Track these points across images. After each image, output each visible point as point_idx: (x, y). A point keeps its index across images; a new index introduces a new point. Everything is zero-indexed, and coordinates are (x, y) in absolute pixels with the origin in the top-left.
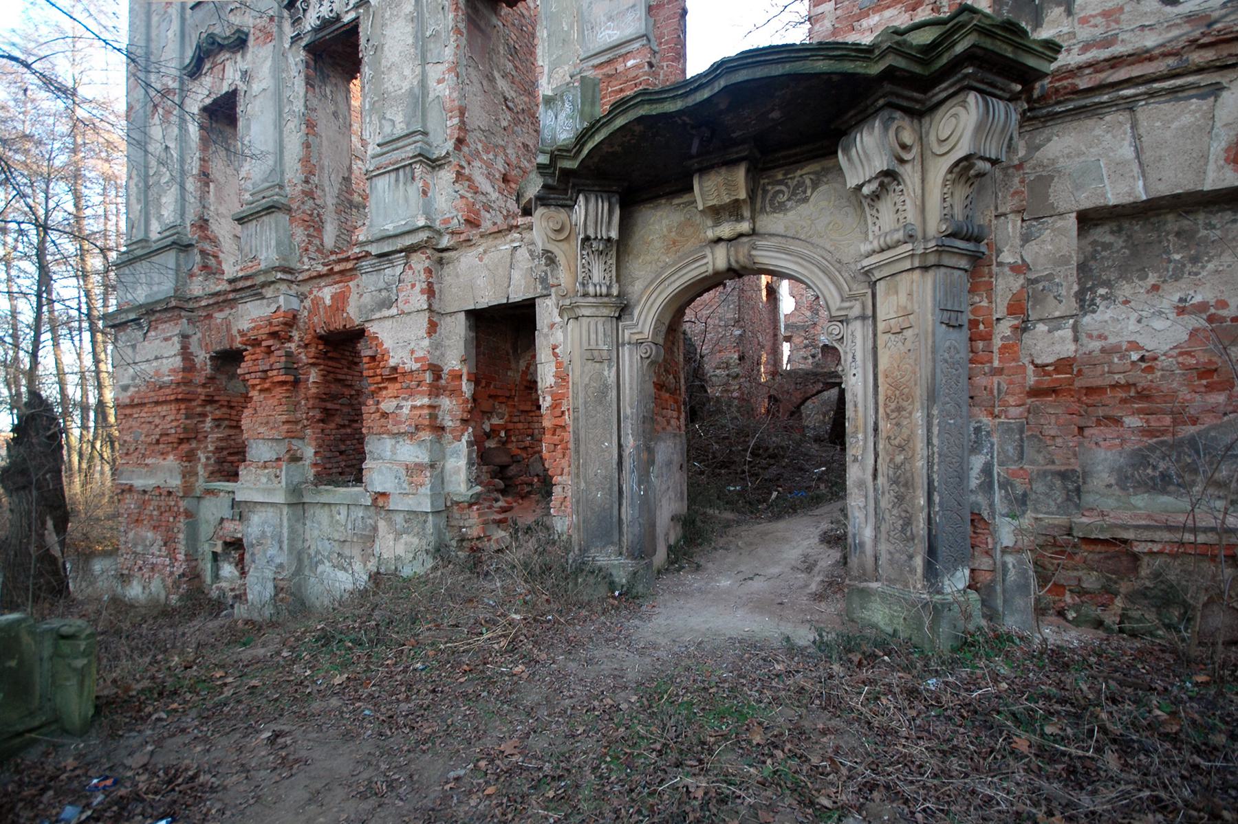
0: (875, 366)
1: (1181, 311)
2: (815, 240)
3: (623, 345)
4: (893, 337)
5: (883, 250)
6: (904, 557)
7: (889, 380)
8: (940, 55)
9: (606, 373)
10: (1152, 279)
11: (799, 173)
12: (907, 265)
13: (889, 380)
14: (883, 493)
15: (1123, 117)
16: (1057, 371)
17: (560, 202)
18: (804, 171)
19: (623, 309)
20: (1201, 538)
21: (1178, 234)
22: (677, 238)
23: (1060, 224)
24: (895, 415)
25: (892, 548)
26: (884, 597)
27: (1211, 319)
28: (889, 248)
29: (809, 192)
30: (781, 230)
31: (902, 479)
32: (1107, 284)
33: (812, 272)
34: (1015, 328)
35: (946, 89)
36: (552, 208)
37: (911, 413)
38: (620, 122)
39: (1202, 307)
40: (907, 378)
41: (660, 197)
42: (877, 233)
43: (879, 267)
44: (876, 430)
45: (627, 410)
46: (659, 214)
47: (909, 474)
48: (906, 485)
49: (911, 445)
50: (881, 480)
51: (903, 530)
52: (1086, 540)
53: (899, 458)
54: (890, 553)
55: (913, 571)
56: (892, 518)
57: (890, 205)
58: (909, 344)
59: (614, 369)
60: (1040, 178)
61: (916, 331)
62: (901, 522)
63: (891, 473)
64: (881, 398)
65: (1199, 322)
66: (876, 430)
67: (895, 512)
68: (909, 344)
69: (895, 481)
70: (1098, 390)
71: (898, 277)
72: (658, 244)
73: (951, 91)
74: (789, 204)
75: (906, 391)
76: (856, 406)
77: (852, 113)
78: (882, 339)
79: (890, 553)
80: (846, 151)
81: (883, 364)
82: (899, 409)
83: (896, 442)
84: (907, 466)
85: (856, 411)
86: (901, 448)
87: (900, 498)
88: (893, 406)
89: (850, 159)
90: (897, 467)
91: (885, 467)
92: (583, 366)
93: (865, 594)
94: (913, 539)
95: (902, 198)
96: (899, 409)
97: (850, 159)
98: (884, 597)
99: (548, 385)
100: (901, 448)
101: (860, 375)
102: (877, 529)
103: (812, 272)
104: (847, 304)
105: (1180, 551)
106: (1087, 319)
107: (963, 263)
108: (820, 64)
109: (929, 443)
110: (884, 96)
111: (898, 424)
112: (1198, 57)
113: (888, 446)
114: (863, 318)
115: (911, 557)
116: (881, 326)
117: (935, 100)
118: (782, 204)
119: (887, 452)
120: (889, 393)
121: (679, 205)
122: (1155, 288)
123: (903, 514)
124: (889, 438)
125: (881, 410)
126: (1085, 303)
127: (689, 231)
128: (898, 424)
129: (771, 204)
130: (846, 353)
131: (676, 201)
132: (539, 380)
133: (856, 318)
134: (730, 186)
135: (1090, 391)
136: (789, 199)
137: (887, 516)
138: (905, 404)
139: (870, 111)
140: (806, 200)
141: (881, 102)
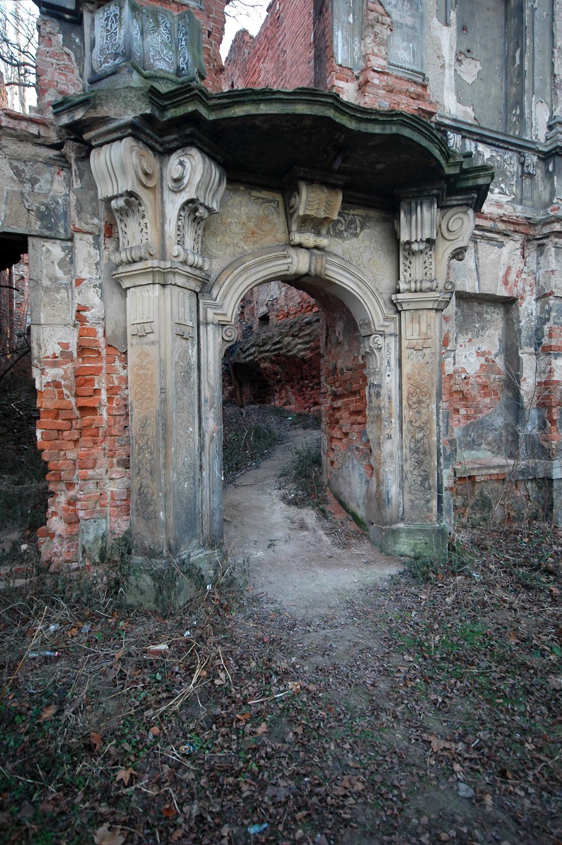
3: (207, 324)
4: (415, 352)
5: (416, 291)
6: (423, 502)
7: (411, 382)
8: (468, 179)
9: (190, 352)
10: (470, 336)
11: (352, 212)
12: (430, 305)
13: (411, 382)
14: (406, 460)
17: (150, 142)
18: (355, 212)
19: (204, 286)
20: (495, 471)
21: (478, 314)
22: (255, 229)
24: (415, 406)
25: (413, 497)
26: (409, 532)
27: (486, 360)
28: (421, 291)
29: (358, 229)
31: (421, 450)
33: (365, 293)
35: (458, 200)
36: (141, 145)
37: (428, 405)
38: (301, 109)
40: (426, 381)
41: (241, 182)
42: (408, 278)
43: (409, 302)
45: (206, 393)
47: (427, 446)
48: (425, 453)
49: (429, 426)
51: (422, 484)
53: (419, 436)
54: (411, 501)
55: (430, 510)
56: (413, 477)
57: (421, 262)
58: (427, 359)
59: (196, 348)
61: (433, 351)
62: (420, 479)
63: (412, 445)
64: (405, 394)
65: (482, 360)
67: (416, 472)
68: (427, 359)
71: (420, 312)
72: (235, 228)
73: (460, 202)
74: (345, 234)
75: (425, 390)
76: (390, 398)
77: (414, 189)
79: (411, 501)
80: (409, 213)
81: (406, 370)
82: (419, 402)
83: (417, 424)
84: (426, 441)
85: (390, 402)
86: (421, 428)
87: (420, 463)
88: (414, 399)
90: (418, 441)
91: (407, 442)
92: (174, 341)
93: (395, 533)
94: (430, 489)
95: (430, 260)
96: (419, 402)
98: (409, 532)
99: (50, 353)
100: (421, 428)
101: (393, 376)
102: (402, 488)
103: (365, 293)
104: (386, 323)
105: (491, 479)
107: (193, 285)
108: (437, 151)
109: (438, 425)
110: (439, 189)
111: (418, 412)
112: (501, 226)
113: (410, 427)
114: (396, 336)
115: (428, 501)
116: (405, 343)
117: (449, 203)
118: (341, 232)
119: (409, 431)
120: (411, 390)
121: (258, 198)
123: (422, 473)
124: (411, 422)
125: (404, 402)
127: (267, 227)
128: (418, 412)
130: (382, 358)
131: (255, 193)
132: (34, 345)
133: (391, 335)
134: (329, 206)
136: (345, 230)
137: (409, 476)
138: (424, 399)
139: (425, 194)
140: (356, 235)
141: (435, 192)
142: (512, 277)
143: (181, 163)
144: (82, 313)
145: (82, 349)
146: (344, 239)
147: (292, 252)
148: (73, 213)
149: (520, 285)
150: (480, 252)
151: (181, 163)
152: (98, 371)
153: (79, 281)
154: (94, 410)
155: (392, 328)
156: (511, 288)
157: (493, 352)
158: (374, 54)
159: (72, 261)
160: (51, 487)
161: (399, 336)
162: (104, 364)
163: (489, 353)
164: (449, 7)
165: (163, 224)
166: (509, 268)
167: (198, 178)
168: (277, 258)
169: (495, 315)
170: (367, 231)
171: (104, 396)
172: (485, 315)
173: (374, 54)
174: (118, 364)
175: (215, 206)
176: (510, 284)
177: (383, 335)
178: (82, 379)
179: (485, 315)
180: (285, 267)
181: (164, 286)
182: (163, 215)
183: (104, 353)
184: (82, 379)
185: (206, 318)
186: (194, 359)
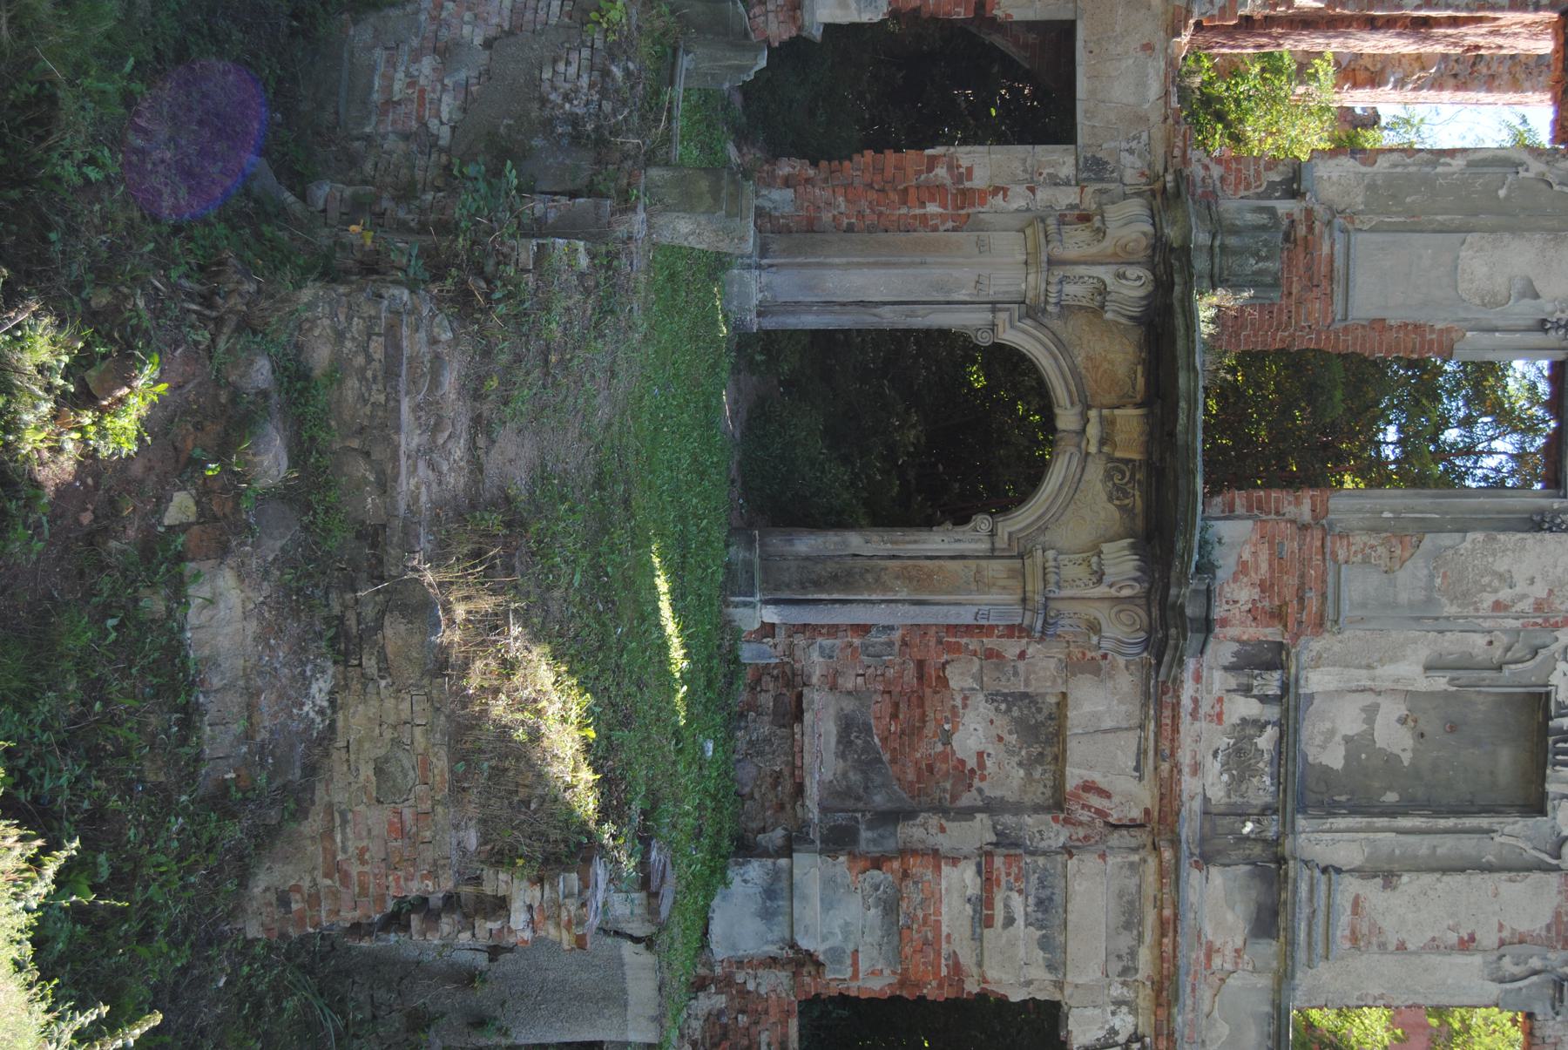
0: (939, 303)
1: (980, 754)
2: (1072, 506)
3: (994, 311)
11: (1137, 493)
15: (1135, 722)
16: (938, 677)
21: (1041, 754)
23: (1059, 681)
27: (972, 771)
30: (1086, 477)
32: (1009, 710)
34: (147, 725)
39: (982, 765)
44: (894, 557)
46: (1130, 350)
50: (850, 562)
52: (800, 696)
53: (870, 578)
59: (968, 299)
60: (1100, 669)
66: (894, 557)
69: (849, 573)
70: (921, 705)
78: (972, 564)
89: (1123, 549)
97: (1123, 549)
106: (981, 697)
114: (993, 549)
116: (983, 563)
122: (1000, 739)
125: (910, 562)
126: (992, 697)
129: (1113, 468)
131: (1140, 369)
135: (921, 699)
140: (1110, 499)
142: (1095, 801)
143: (1139, 278)
144: (1001, 195)
145: (964, 192)
146: (1104, 482)
147: (1078, 409)
148: (1099, 186)
149: (1084, 816)
150: (1125, 734)
151: (1139, 278)
152: (944, 207)
153: (1032, 190)
154: (904, 202)
155: (1002, 542)
156: (1079, 797)
157: (984, 785)
158: (1349, 544)
159: (1056, 184)
160: (823, 164)
161: (992, 555)
162: (950, 211)
163: (983, 778)
164: (1455, 674)
165: (1085, 263)
166: (1108, 796)
167: (1125, 291)
168: (1069, 391)
169: (1042, 789)
170: (1117, 515)
171: (918, 211)
172: (1040, 769)
173: (1349, 544)
174: (950, 224)
175: (1109, 316)
176: (1085, 795)
177: (993, 534)
178: (935, 191)
179: (1040, 769)
180: (1062, 402)
181: (1026, 263)
182: (1094, 263)
183: (963, 212)
184: (935, 191)
185: (1000, 310)
186: (956, 297)
